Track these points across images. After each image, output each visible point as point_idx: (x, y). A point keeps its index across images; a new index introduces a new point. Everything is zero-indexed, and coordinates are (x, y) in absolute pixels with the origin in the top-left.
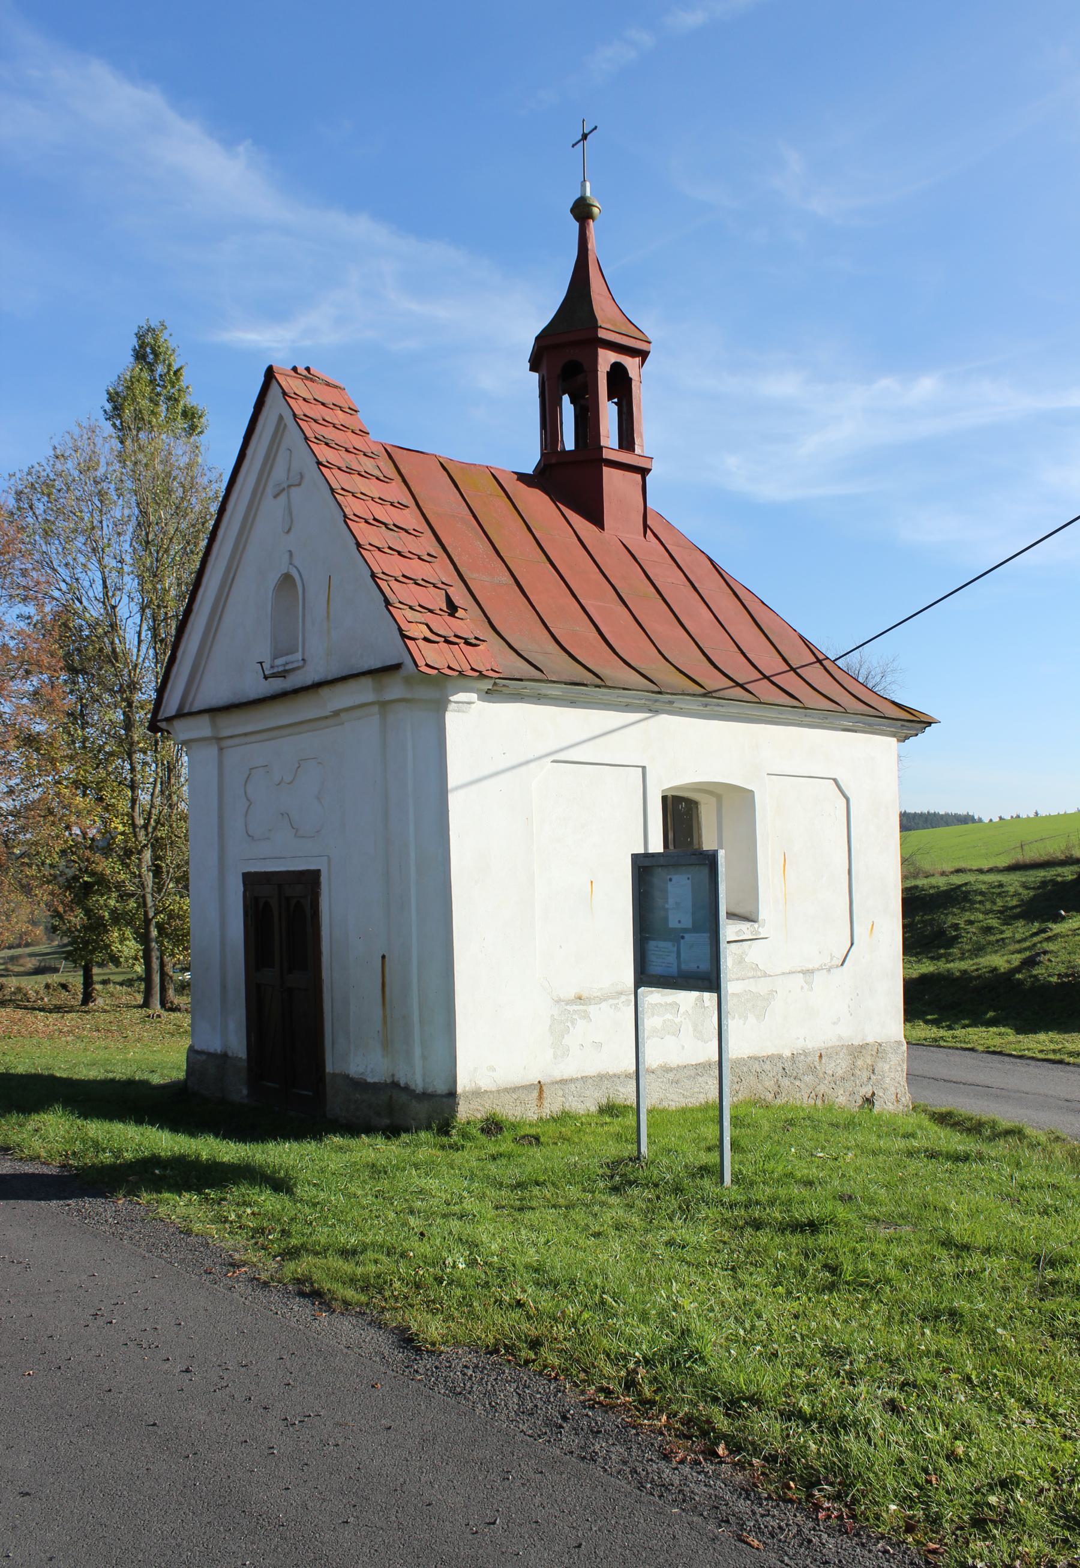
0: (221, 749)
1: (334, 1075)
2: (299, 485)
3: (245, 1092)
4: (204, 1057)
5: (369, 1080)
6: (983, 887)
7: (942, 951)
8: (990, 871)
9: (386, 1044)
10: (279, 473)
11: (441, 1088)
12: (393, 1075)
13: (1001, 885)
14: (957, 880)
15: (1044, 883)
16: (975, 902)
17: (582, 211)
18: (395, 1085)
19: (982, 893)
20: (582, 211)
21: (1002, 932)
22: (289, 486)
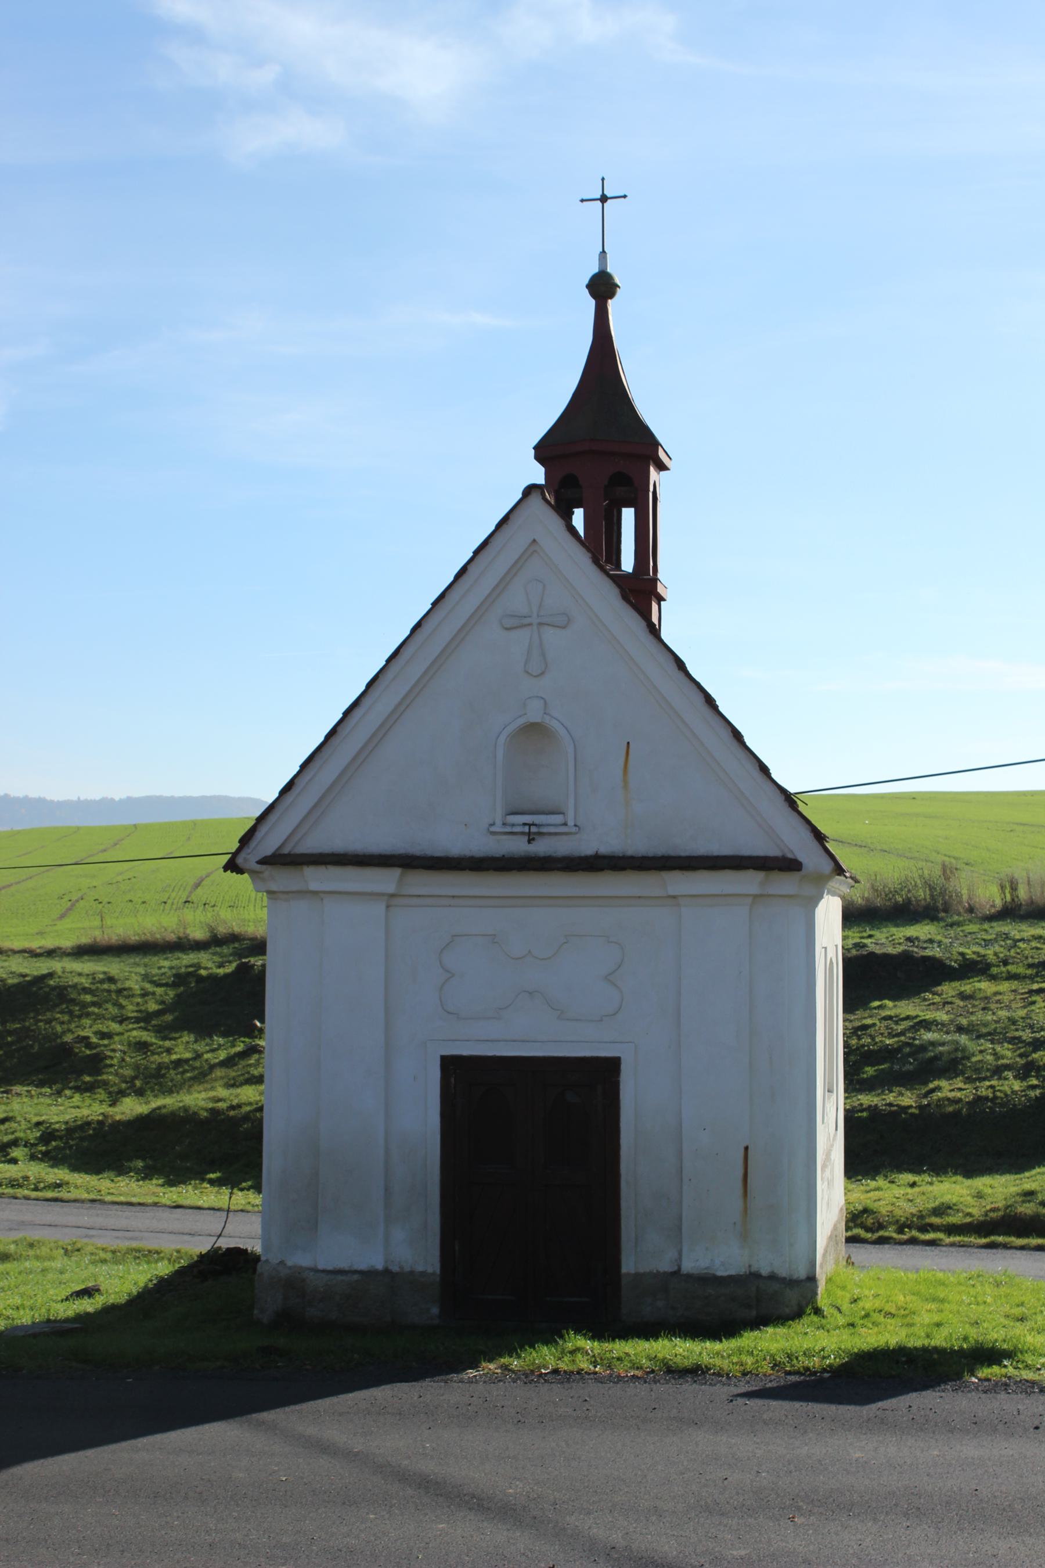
0: (388, 907)
1: (638, 1276)
2: (564, 627)
3: (435, 1310)
4: (356, 1277)
5: (719, 1273)
6: (85, 982)
7: (87, 1079)
8: (82, 952)
9: (744, 1236)
10: (516, 600)
11: (802, 1273)
12: (750, 1266)
13: (111, 980)
14: (42, 967)
15: (180, 979)
16: (84, 1005)
17: (602, 287)
18: (756, 1276)
19: (86, 991)
20: (602, 287)
21: (169, 1051)
22: (540, 624)
